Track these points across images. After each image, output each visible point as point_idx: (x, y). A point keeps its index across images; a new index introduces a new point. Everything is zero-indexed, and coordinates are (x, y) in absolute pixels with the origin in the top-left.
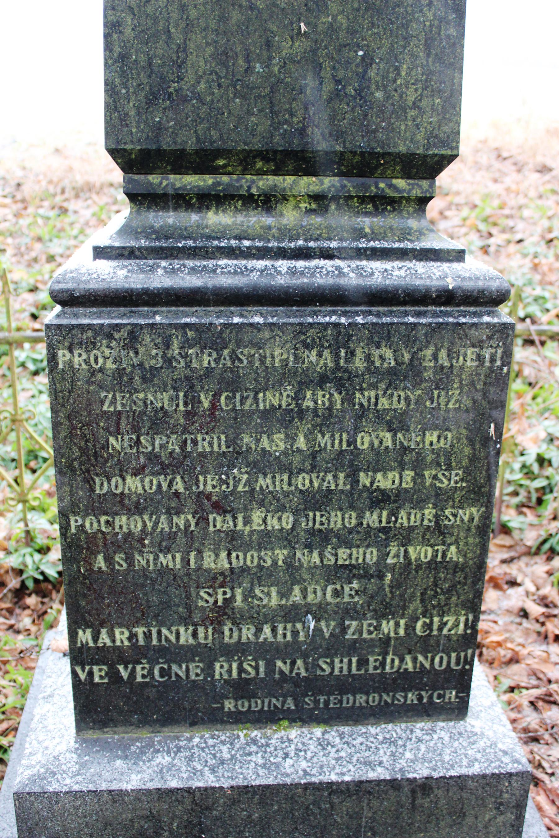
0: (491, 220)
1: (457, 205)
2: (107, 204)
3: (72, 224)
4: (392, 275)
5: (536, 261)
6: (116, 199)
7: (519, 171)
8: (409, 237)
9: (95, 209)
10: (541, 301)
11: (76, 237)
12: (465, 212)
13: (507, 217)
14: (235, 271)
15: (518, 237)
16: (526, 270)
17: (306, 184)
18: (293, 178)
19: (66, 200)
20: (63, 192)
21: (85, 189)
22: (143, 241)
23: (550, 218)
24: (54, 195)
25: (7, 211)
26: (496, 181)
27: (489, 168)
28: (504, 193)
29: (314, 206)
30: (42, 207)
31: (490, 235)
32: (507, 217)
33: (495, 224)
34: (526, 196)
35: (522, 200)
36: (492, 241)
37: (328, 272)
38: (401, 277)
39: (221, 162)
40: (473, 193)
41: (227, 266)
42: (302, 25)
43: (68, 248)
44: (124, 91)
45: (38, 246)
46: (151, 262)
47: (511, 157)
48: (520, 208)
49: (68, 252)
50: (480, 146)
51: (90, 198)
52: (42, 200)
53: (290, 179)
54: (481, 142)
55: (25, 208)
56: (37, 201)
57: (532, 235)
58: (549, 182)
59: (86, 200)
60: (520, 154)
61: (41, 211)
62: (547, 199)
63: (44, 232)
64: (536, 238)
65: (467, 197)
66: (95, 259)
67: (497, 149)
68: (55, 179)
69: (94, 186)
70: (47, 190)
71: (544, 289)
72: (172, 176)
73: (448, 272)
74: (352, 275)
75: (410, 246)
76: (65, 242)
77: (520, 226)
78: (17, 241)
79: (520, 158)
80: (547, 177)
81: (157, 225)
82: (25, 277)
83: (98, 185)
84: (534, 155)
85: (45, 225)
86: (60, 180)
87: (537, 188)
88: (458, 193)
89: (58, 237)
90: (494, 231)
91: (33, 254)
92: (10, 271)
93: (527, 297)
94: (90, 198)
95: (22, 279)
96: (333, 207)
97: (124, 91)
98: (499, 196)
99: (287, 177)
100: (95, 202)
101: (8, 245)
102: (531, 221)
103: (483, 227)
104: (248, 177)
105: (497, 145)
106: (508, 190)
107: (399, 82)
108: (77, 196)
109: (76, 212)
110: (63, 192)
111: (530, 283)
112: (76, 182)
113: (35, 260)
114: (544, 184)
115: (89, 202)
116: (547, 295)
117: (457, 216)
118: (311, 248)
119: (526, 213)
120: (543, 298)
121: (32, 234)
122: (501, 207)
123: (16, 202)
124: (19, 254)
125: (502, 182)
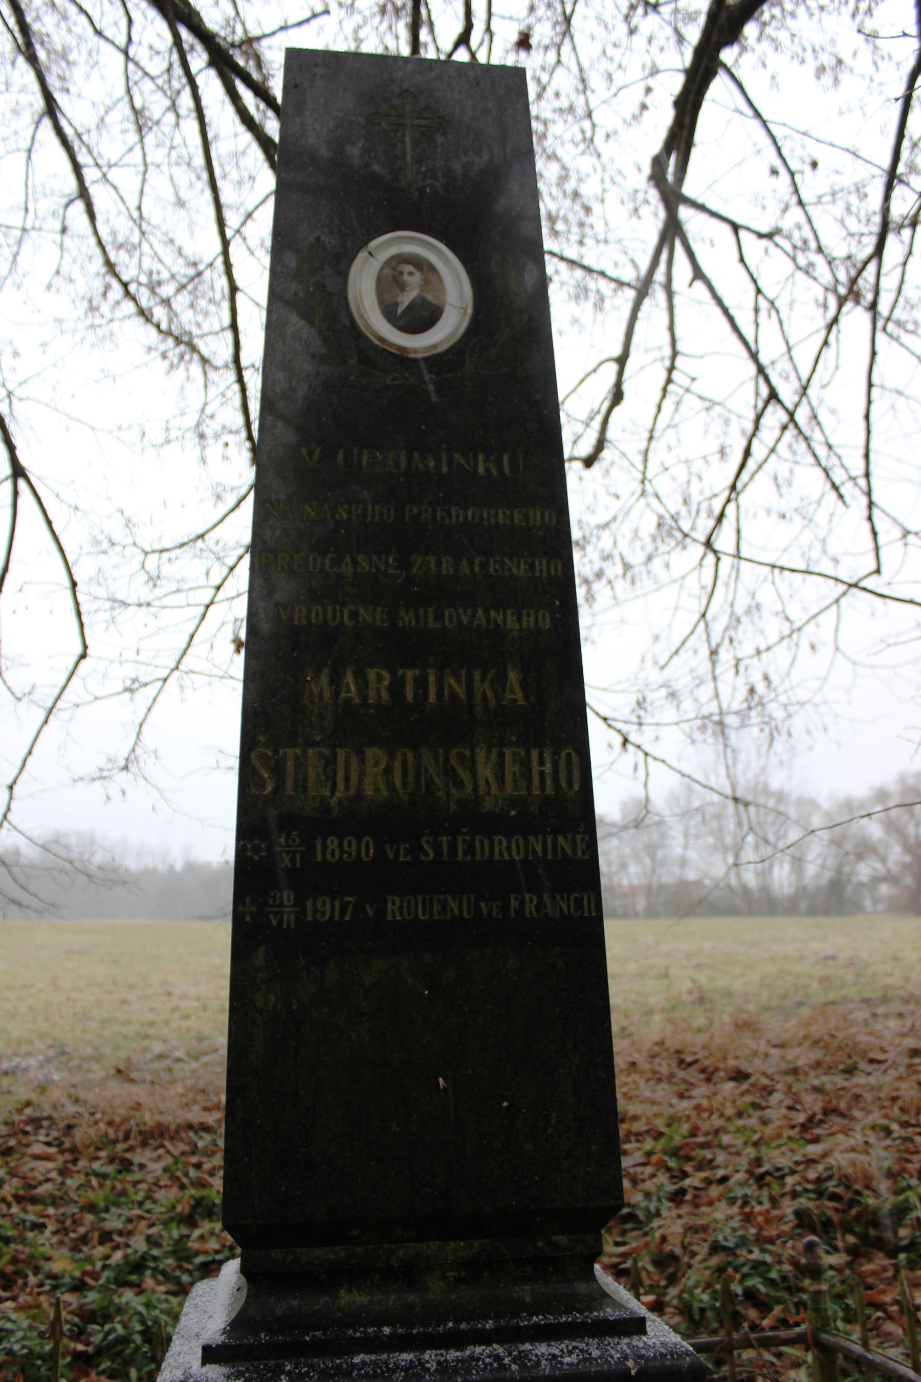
0: (682, 1153)
1: (638, 1134)
2: (183, 1153)
3: (135, 1184)
4: (561, 1363)
5: (747, 1210)
6: (196, 1146)
7: (708, 1080)
8: (578, 1305)
9: (169, 1160)
10: (762, 1269)
11: (141, 1204)
12: (649, 1144)
13: (703, 1146)
14: (375, 1372)
15: (720, 1173)
16: (735, 1223)
17: (456, 1248)
18: (437, 1243)
19: (131, 1149)
20: (127, 1137)
21: (156, 1134)
22: (263, 1335)
23: (756, 1144)
24: (115, 1142)
25: (50, 1165)
26: (681, 1096)
27: (672, 1076)
28: (694, 1113)
29: (463, 1274)
30: (98, 1158)
31: (685, 1175)
32: (703, 1146)
33: (689, 1159)
34: (722, 1115)
35: (717, 1122)
36: (687, 1182)
37: (486, 1365)
38: (573, 1364)
39: (355, 1233)
40: (656, 1115)
41: (364, 1363)
42: (441, 1080)
43: (130, 1220)
44: (246, 1159)
45: (89, 1218)
46: (272, 1363)
47: (696, 1061)
48: (717, 1132)
49: (130, 1227)
50: (656, 1048)
51: (162, 1146)
52: (98, 1149)
53: (434, 1245)
54: (657, 1044)
55: (75, 1161)
56: (92, 1150)
57: (737, 1171)
58: (747, 1092)
59: (156, 1149)
60: (707, 1058)
61: (96, 1166)
62: (749, 1116)
63: (97, 1196)
64: (740, 1176)
65: (648, 1123)
66: (204, 1363)
67: (678, 1052)
68: (117, 1119)
69: (168, 1129)
70: (106, 1134)
71: (763, 1251)
72: (298, 1250)
73: (628, 1351)
74: (514, 1367)
75: (579, 1318)
76: (126, 1212)
77: (721, 1158)
78: (62, 1210)
79: (707, 1063)
80: (745, 1086)
81: (279, 1312)
82: (70, 1267)
83: (172, 1127)
84: (725, 1058)
85: (101, 1186)
86: (125, 1120)
87: (734, 1101)
88: (635, 1118)
89: (117, 1205)
90: (688, 1168)
91: (82, 1230)
92: (48, 1259)
93: (744, 1265)
94: (162, 1146)
95: (64, 1271)
96: (486, 1274)
97: (246, 1159)
98: (688, 1117)
99: (431, 1243)
100: (168, 1152)
101: (48, 1216)
102: (733, 1150)
103: (672, 1163)
104: (387, 1246)
105: (677, 1046)
106: (698, 1108)
107: (549, 1131)
108: (144, 1144)
109: (142, 1166)
110: (127, 1137)
111: (743, 1242)
112: (145, 1124)
113: (84, 1239)
114: (742, 1094)
115: (161, 1151)
116: (768, 1258)
117: (639, 1149)
118: (463, 1331)
119: (725, 1139)
120: (764, 1263)
121: (82, 1201)
122: (693, 1133)
123: (62, 1152)
124: (63, 1230)
125: (690, 1097)
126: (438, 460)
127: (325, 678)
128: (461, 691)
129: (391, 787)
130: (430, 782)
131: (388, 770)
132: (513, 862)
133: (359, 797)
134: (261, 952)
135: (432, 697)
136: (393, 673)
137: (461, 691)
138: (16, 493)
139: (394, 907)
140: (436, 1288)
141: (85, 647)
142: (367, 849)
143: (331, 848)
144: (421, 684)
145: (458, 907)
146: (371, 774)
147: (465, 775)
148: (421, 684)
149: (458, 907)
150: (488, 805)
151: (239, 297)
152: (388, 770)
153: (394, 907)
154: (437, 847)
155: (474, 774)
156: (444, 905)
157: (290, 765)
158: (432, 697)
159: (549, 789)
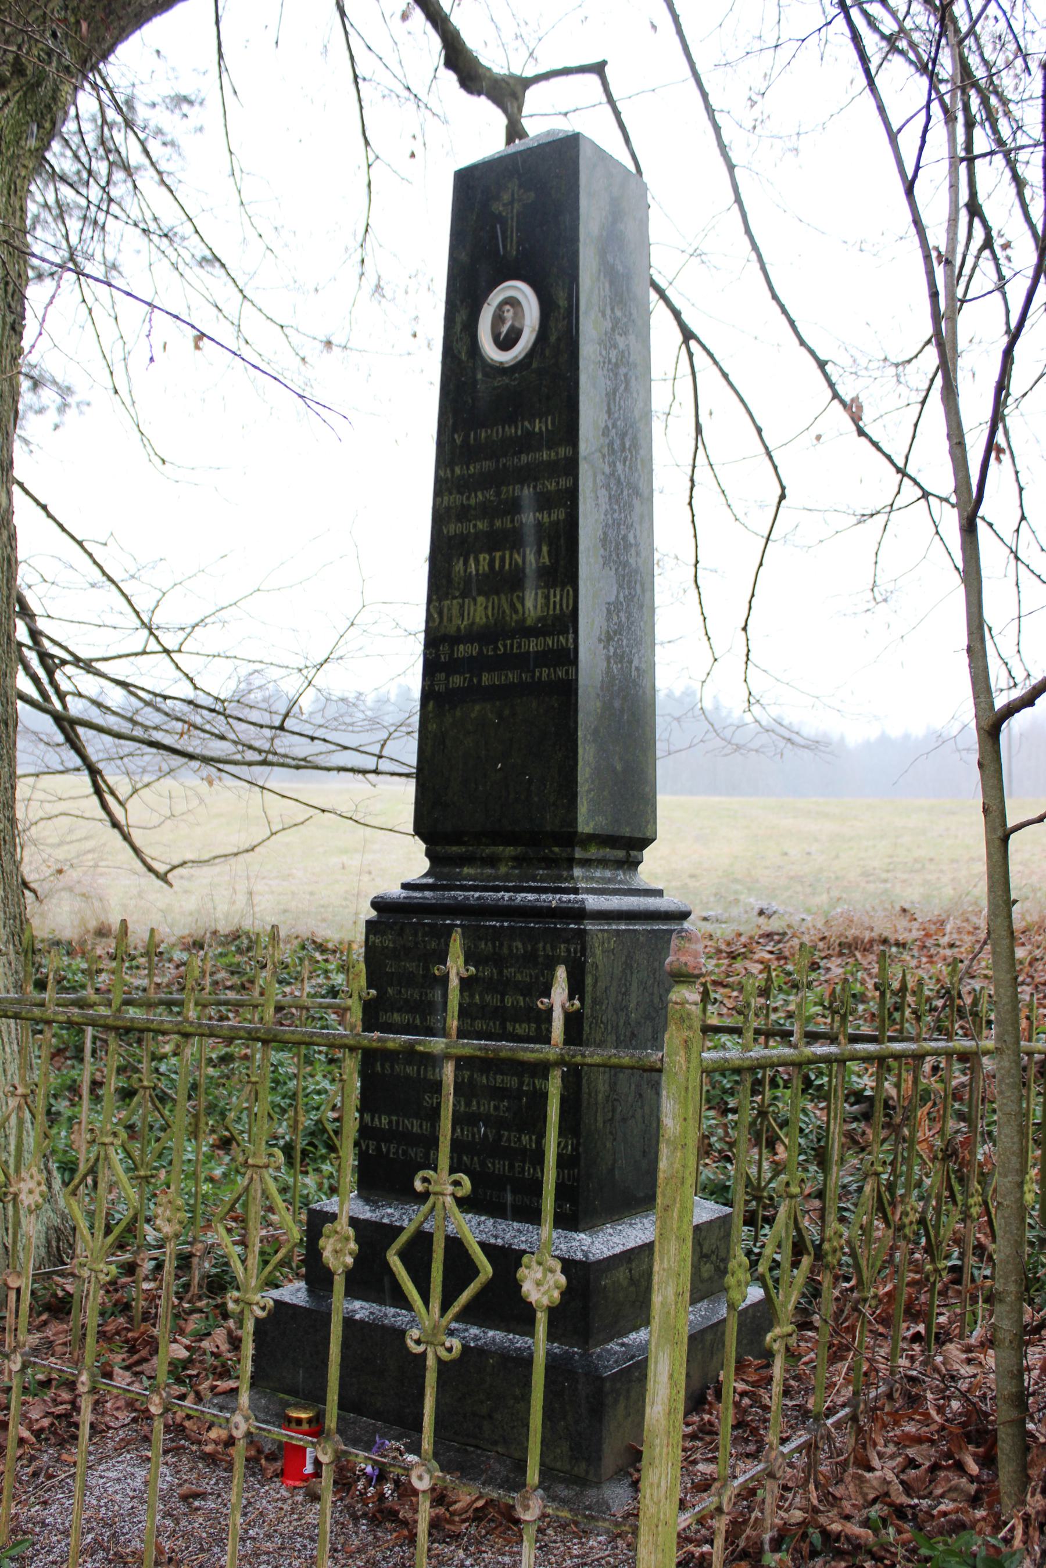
17: (510, 851)
53: (501, 848)
126: (516, 428)
127: (461, 562)
128: (520, 561)
129: (487, 617)
130: (504, 612)
131: (486, 608)
132: (528, 652)
133: (473, 623)
134: (431, 703)
135: (507, 567)
136: (490, 555)
137: (520, 561)
138: (691, 355)
139: (486, 679)
140: (503, 870)
141: (783, 488)
142: (473, 649)
143: (462, 650)
144: (503, 559)
145: (512, 677)
146: (479, 612)
147: (519, 606)
148: (503, 559)
149: (512, 677)
150: (529, 622)
151: (737, 171)
152: (486, 608)
153: (486, 679)
154: (505, 646)
155: (523, 605)
156: (507, 676)
157: (445, 610)
158: (507, 567)
159: (558, 611)
